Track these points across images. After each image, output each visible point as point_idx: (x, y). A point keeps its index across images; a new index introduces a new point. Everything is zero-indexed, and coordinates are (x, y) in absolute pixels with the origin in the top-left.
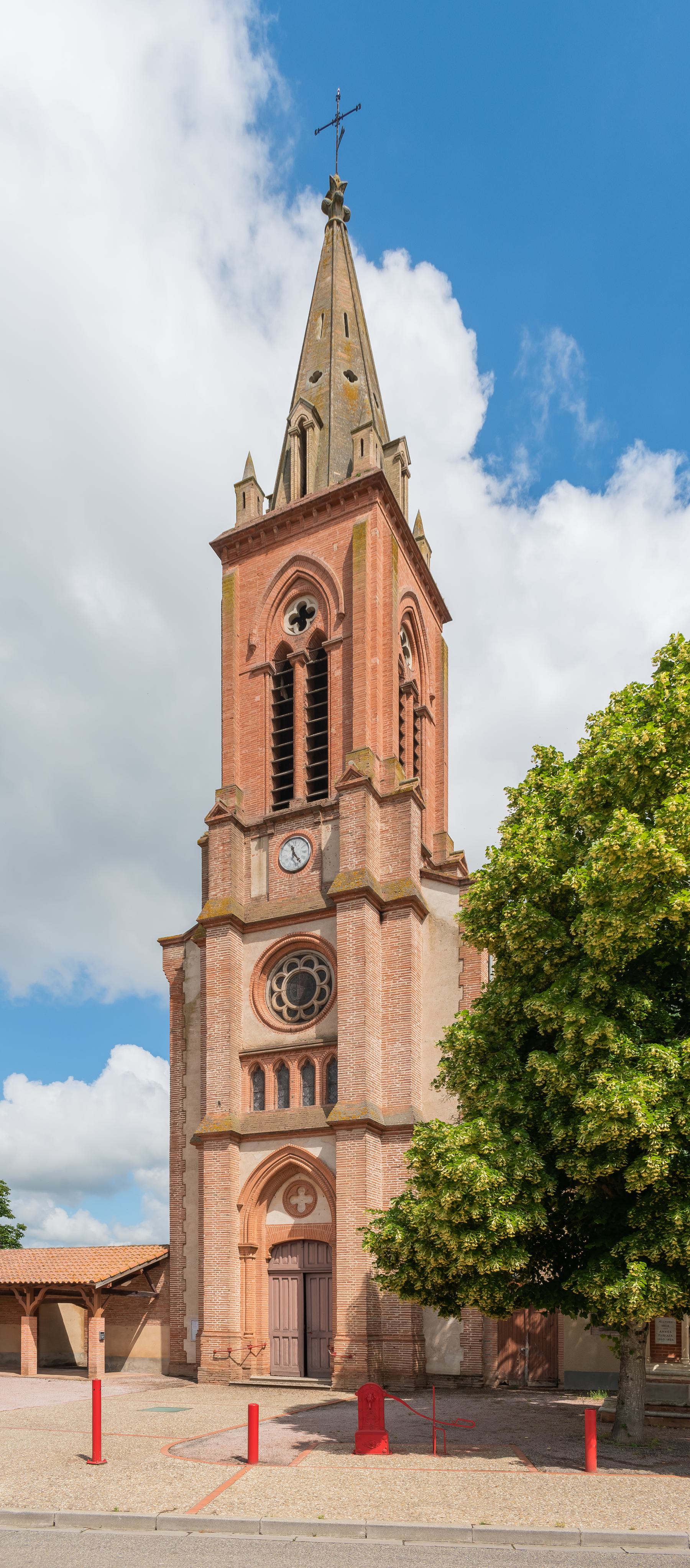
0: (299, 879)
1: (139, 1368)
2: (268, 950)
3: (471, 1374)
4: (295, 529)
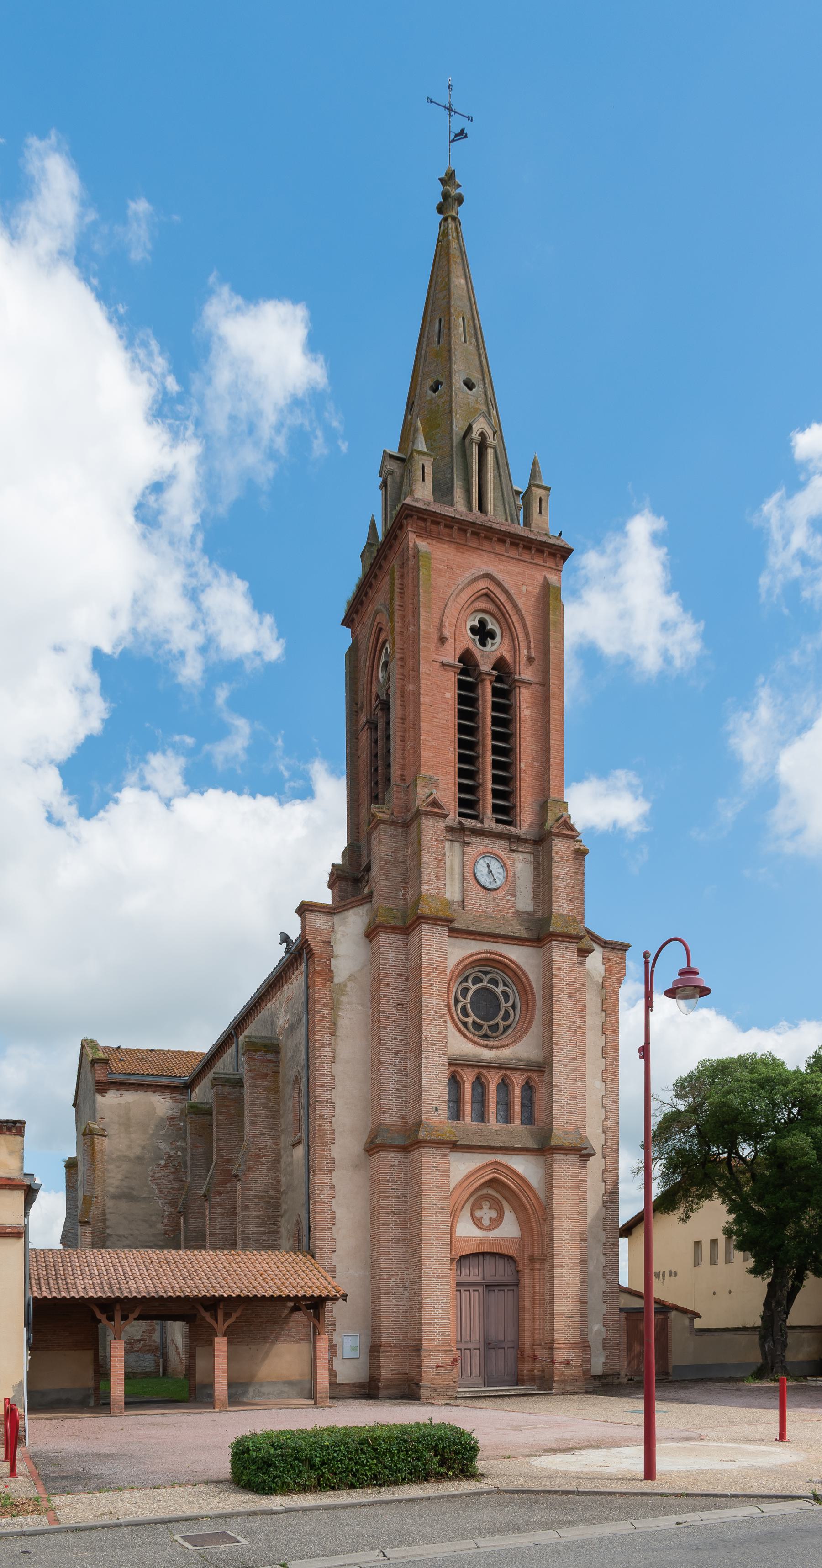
0: (494, 898)
1: (269, 1394)
2: (464, 960)
3: (611, 1373)
4: (486, 545)
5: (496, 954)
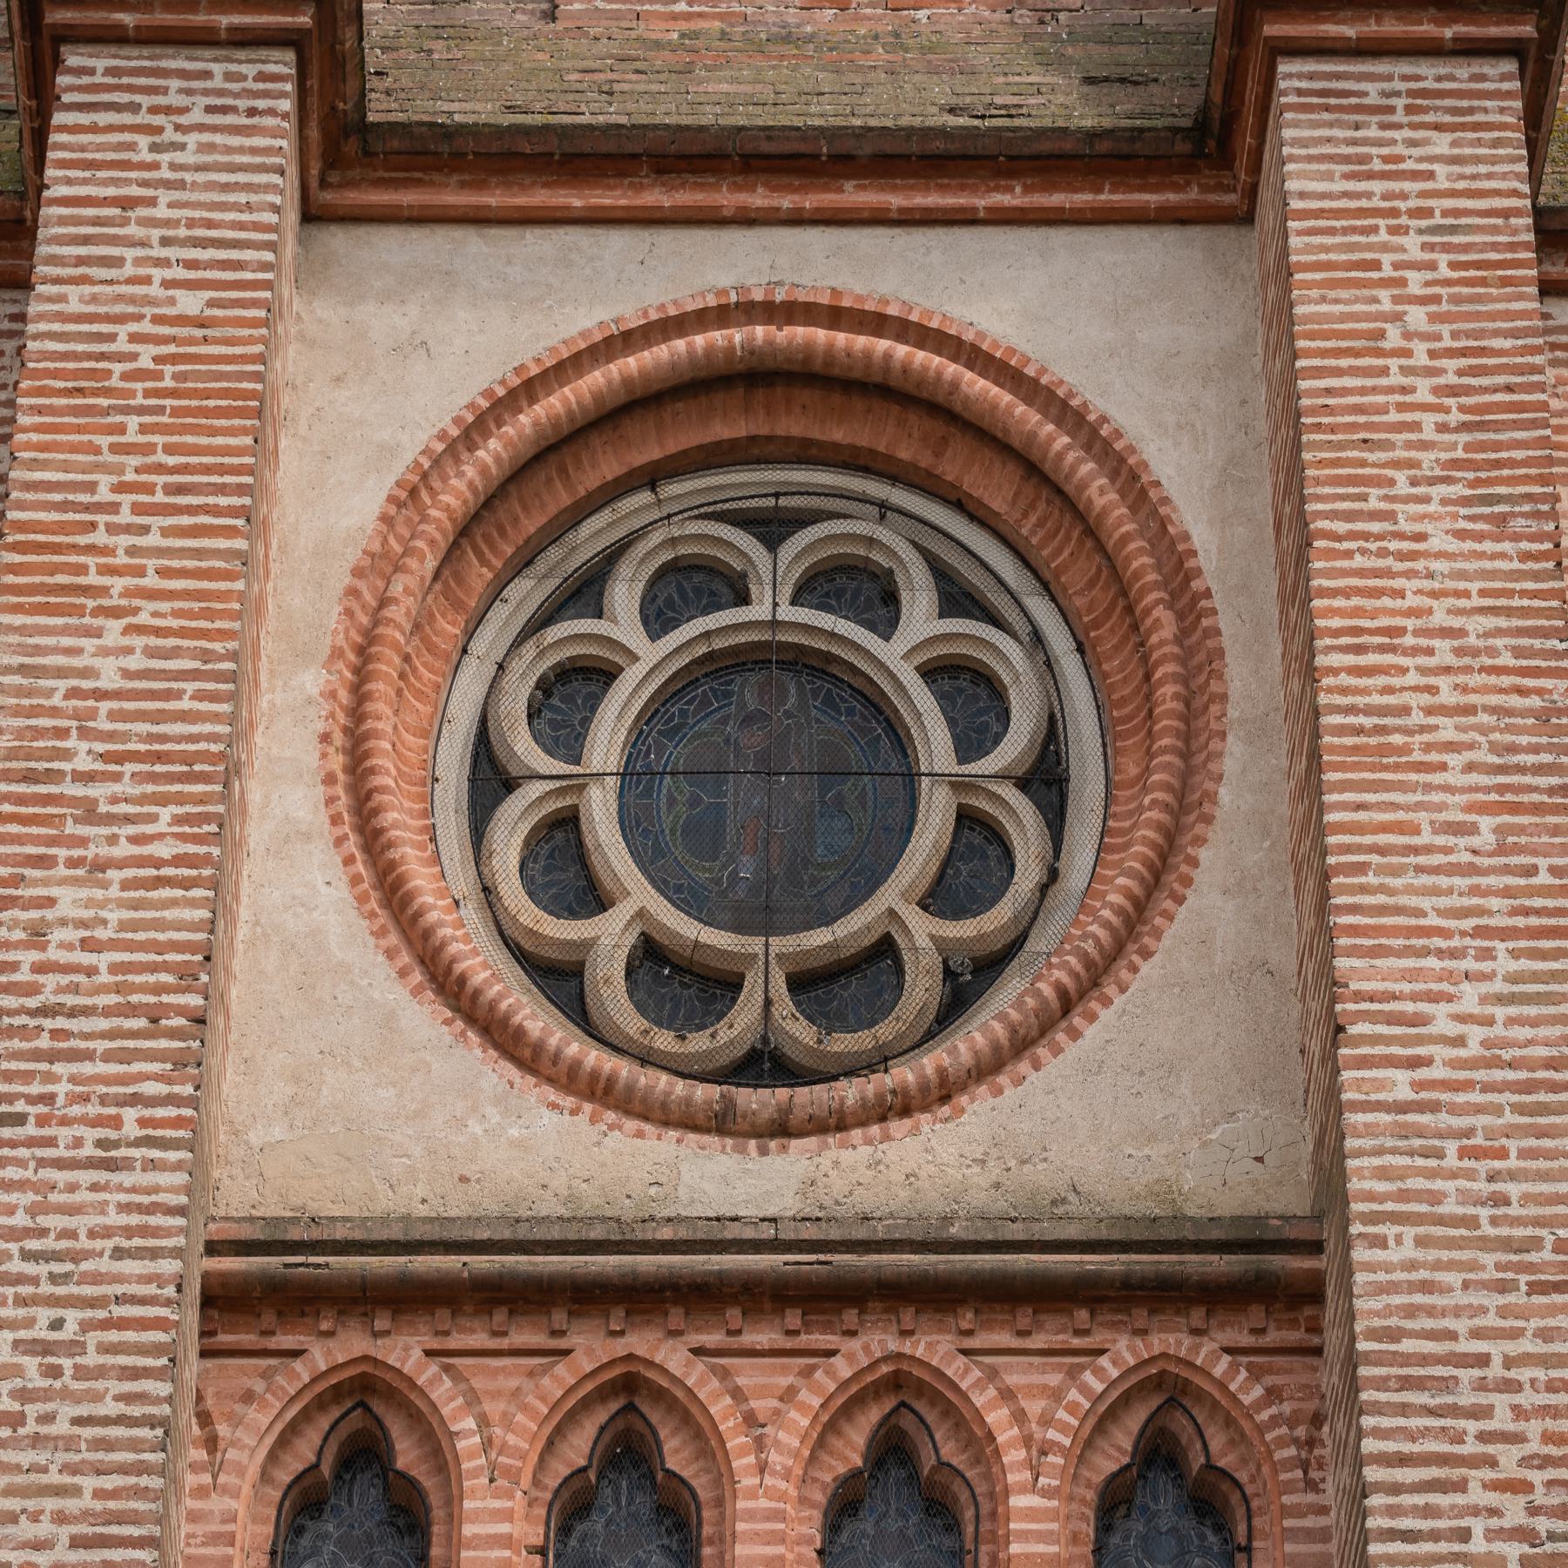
2: (529, 389)
5: (836, 316)
